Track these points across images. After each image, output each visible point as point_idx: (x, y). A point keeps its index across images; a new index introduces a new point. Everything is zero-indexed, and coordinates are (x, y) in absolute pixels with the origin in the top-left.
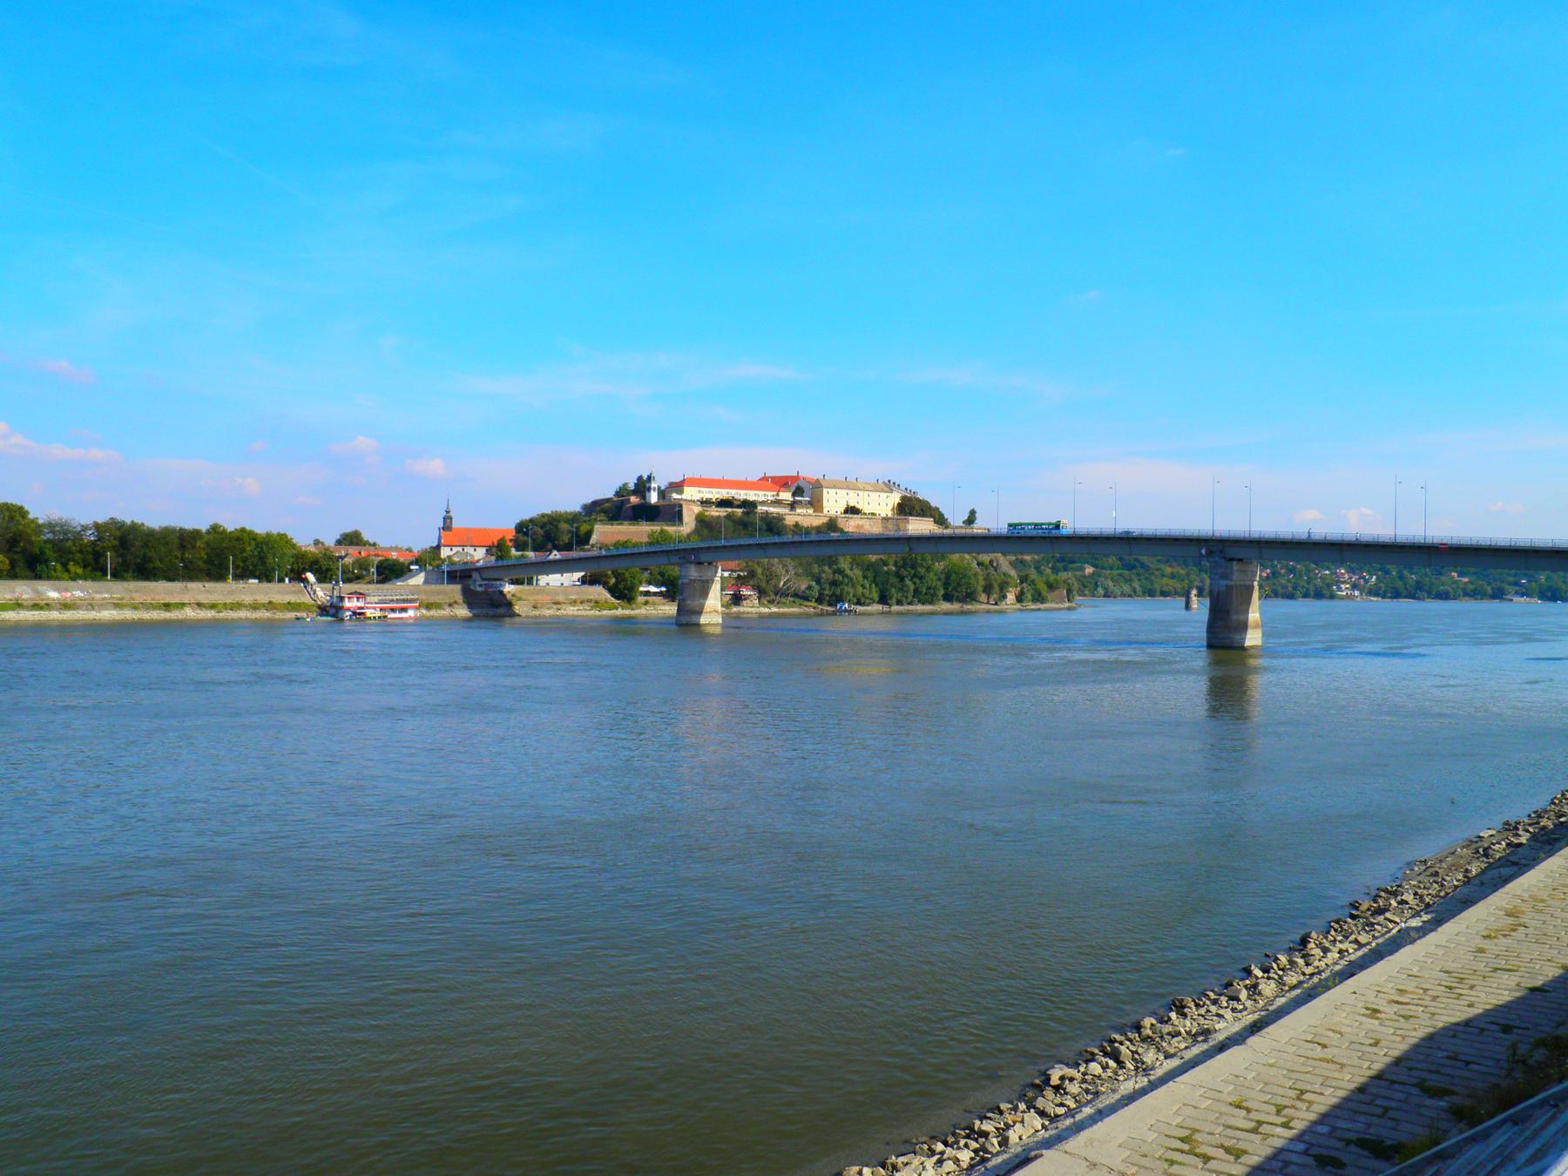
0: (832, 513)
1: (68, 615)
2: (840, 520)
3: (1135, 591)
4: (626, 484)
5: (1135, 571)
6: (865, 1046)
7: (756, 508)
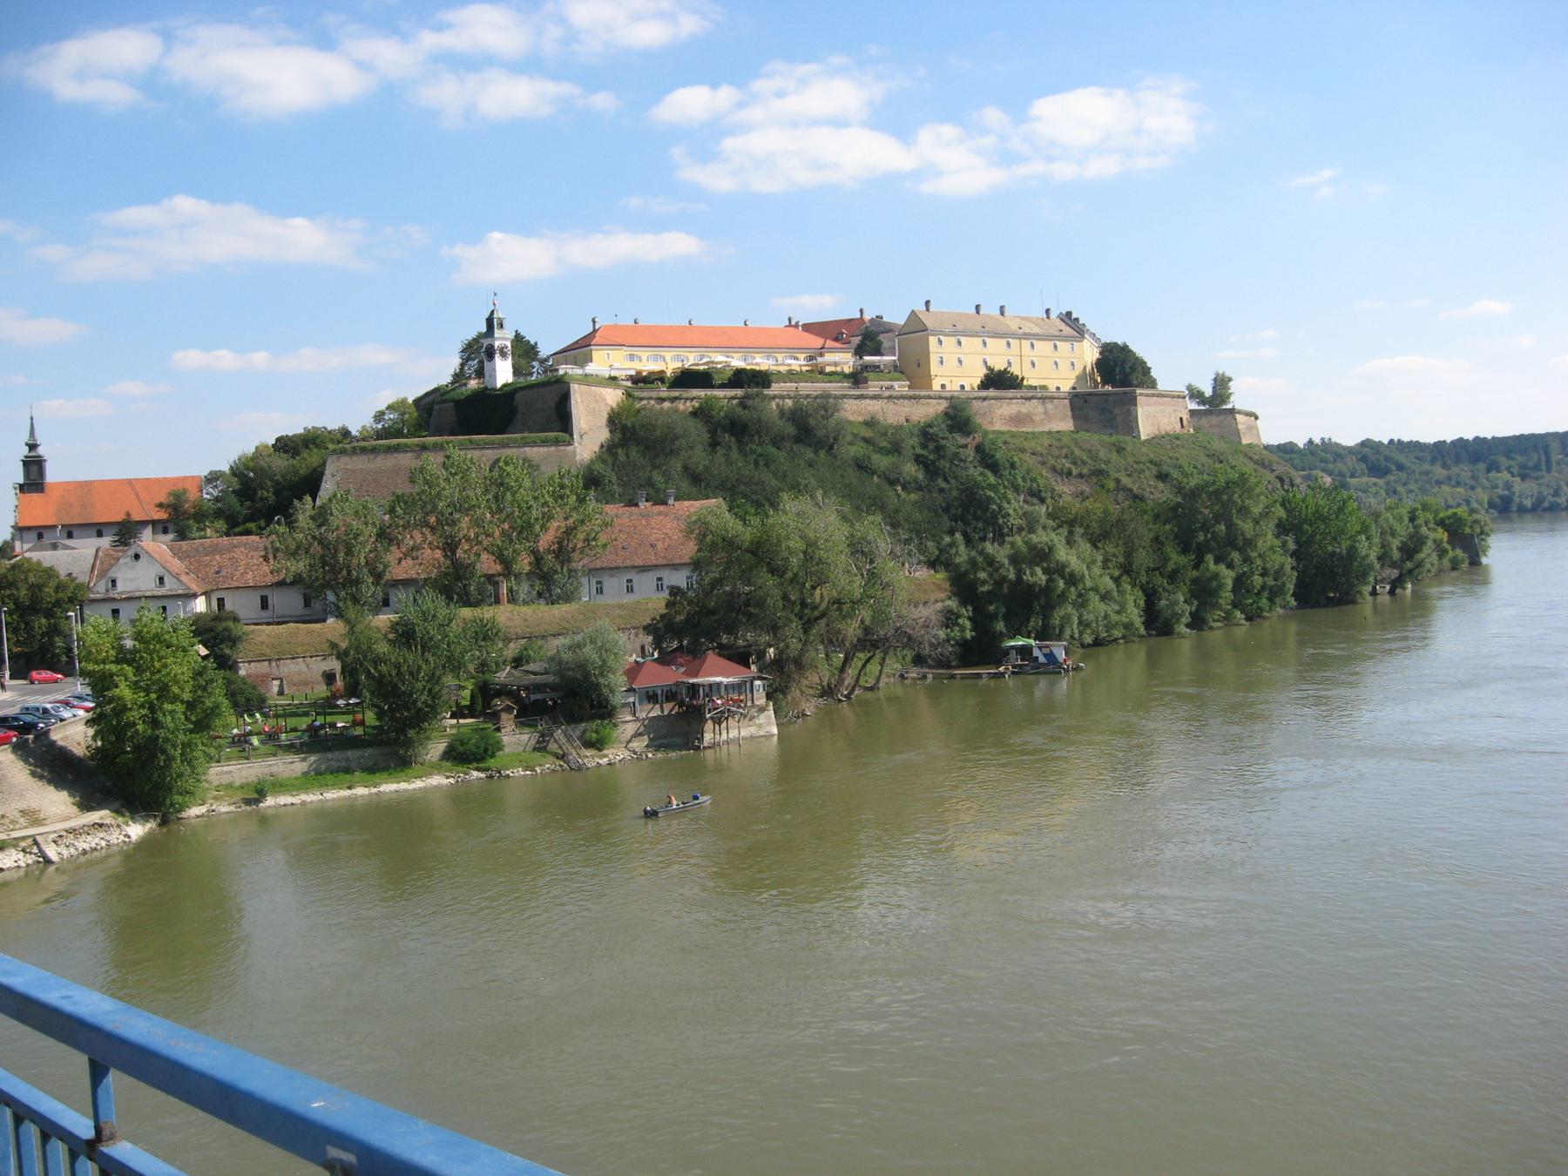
0: (953, 387)
2: (977, 405)
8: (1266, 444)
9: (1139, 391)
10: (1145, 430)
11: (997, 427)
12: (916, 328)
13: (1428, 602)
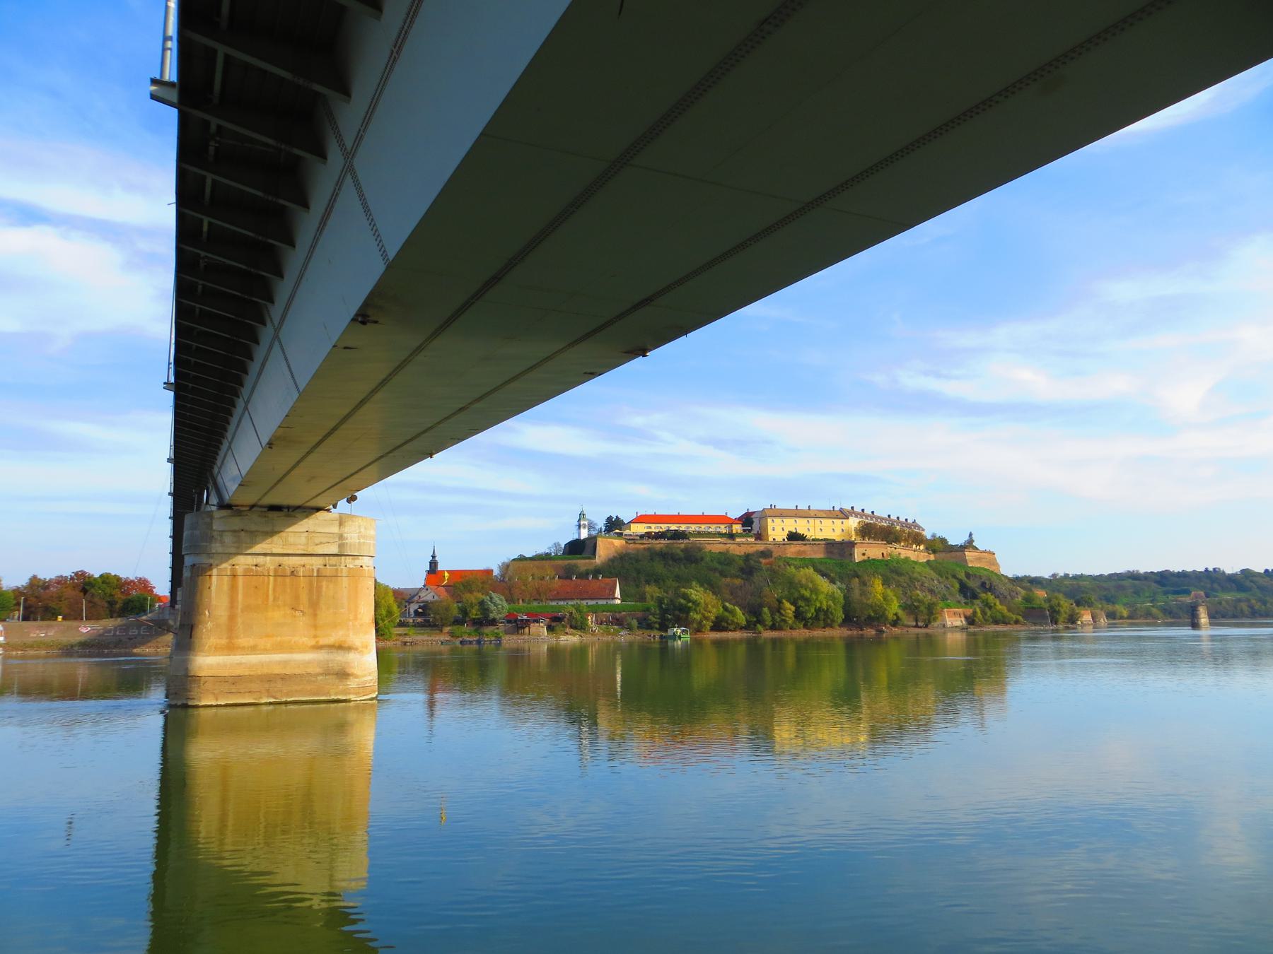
8: (412, 578)
11: (788, 556)
13: (189, 693)
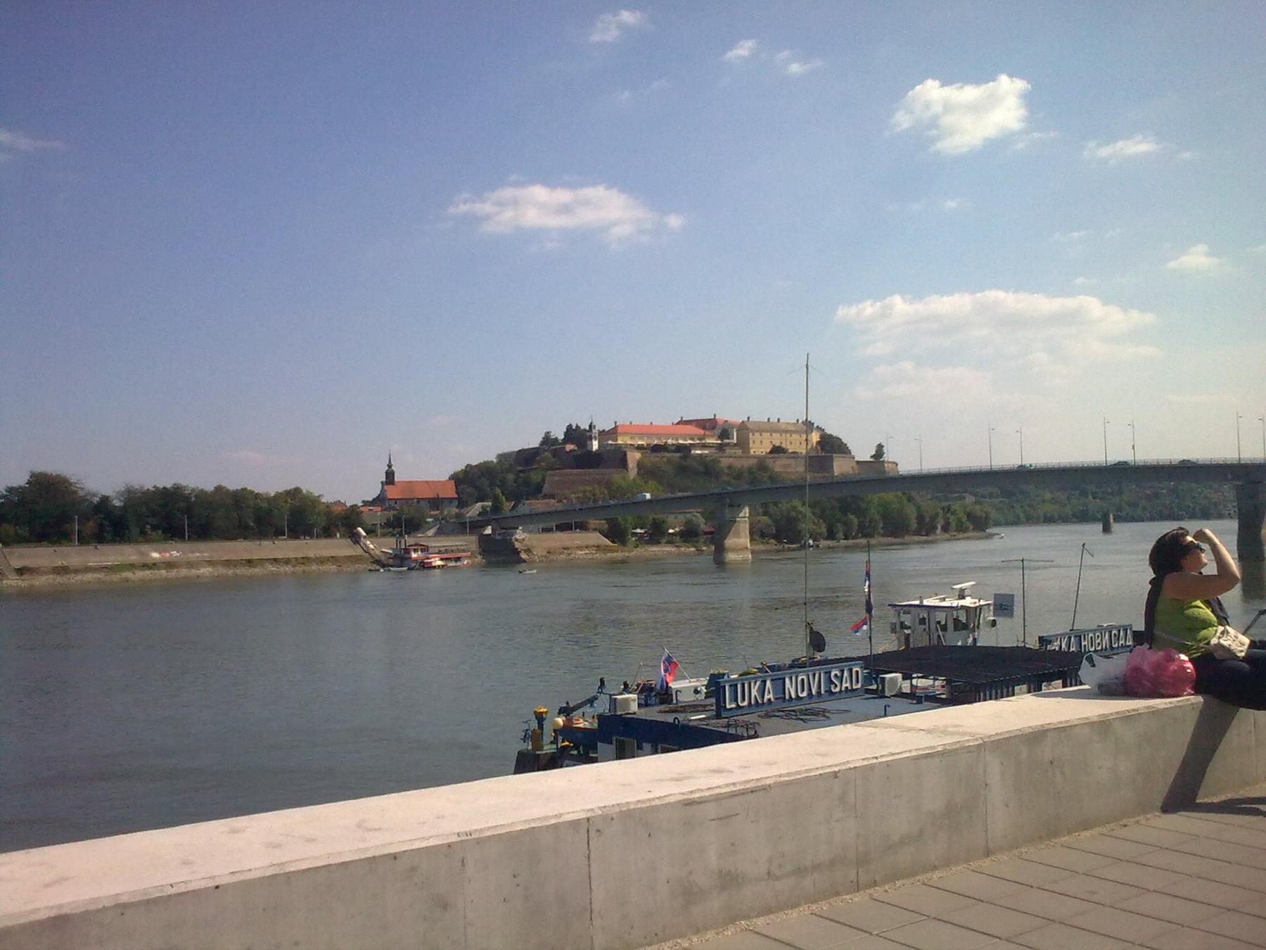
1: (173, 573)
2: (768, 460)
3: (1019, 519)
4: (548, 433)
5: (1014, 498)
6: (760, 922)
7: (690, 451)
9: (834, 455)
10: (837, 471)
12: (743, 428)
